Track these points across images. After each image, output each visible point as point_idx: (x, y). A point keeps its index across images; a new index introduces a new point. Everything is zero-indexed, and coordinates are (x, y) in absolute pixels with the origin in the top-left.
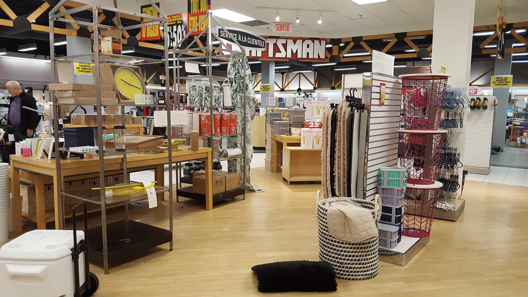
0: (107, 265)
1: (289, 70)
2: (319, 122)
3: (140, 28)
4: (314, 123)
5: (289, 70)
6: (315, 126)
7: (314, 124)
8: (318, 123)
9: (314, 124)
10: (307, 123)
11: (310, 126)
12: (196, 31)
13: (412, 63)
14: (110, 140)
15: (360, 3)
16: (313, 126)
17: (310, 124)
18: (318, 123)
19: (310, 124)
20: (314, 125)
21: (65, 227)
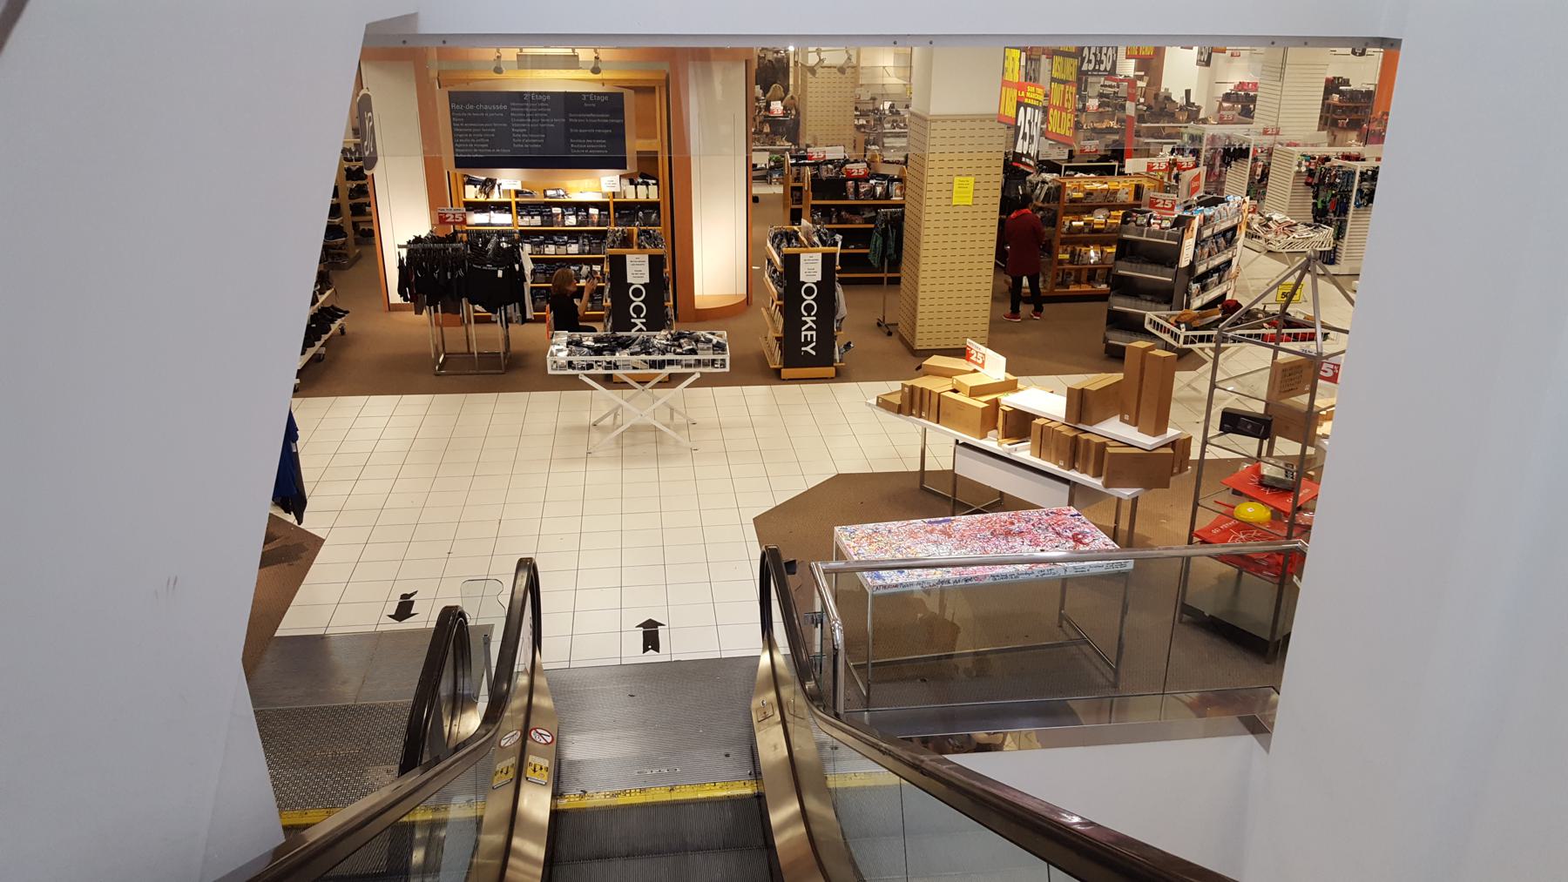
4: (454, 215)
17: (1158, 201)
18: (1332, 367)
19: (1158, 201)
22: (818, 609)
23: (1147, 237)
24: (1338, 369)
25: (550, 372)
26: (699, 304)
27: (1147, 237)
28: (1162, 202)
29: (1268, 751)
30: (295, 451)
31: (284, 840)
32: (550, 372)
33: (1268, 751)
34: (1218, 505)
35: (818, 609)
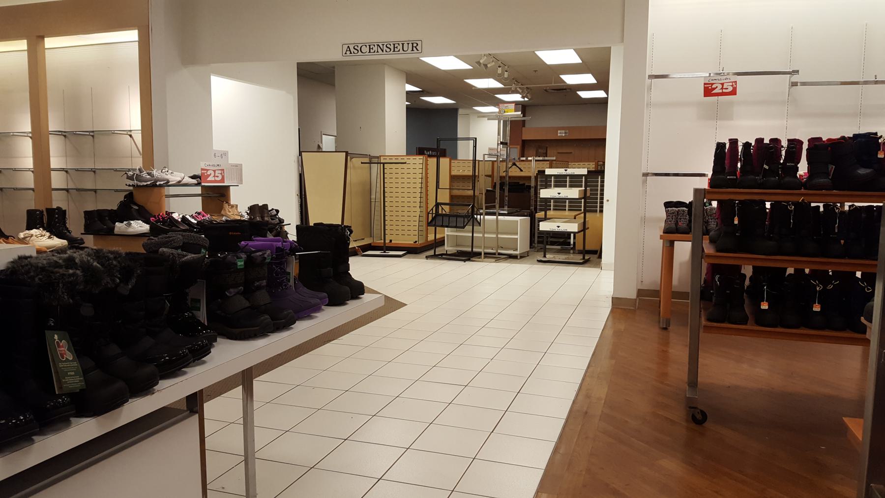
0: (694, 219)
1: (546, 203)
3: (334, 85)
4: (722, 84)
5: (546, 203)
6: (724, 91)
7: (723, 87)
8: (731, 84)
10: (708, 86)
11: (714, 92)
12: (352, 245)
13: (386, 208)
14: (139, 148)
15: (443, 69)
17: (714, 86)
18: (731, 84)
19: (714, 86)
20: (722, 89)
21: (599, 250)
22: (66, 378)
23: (554, 83)
24: (736, 84)
25: (205, 281)
26: (115, 233)
27: (554, 83)
28: (720, 86)
29: (406, 305)
30: (683, 249)
31: (857, 276)
32: (205, 281)
33: (406, 305)
34: (403, 161)
35: (66, 378)
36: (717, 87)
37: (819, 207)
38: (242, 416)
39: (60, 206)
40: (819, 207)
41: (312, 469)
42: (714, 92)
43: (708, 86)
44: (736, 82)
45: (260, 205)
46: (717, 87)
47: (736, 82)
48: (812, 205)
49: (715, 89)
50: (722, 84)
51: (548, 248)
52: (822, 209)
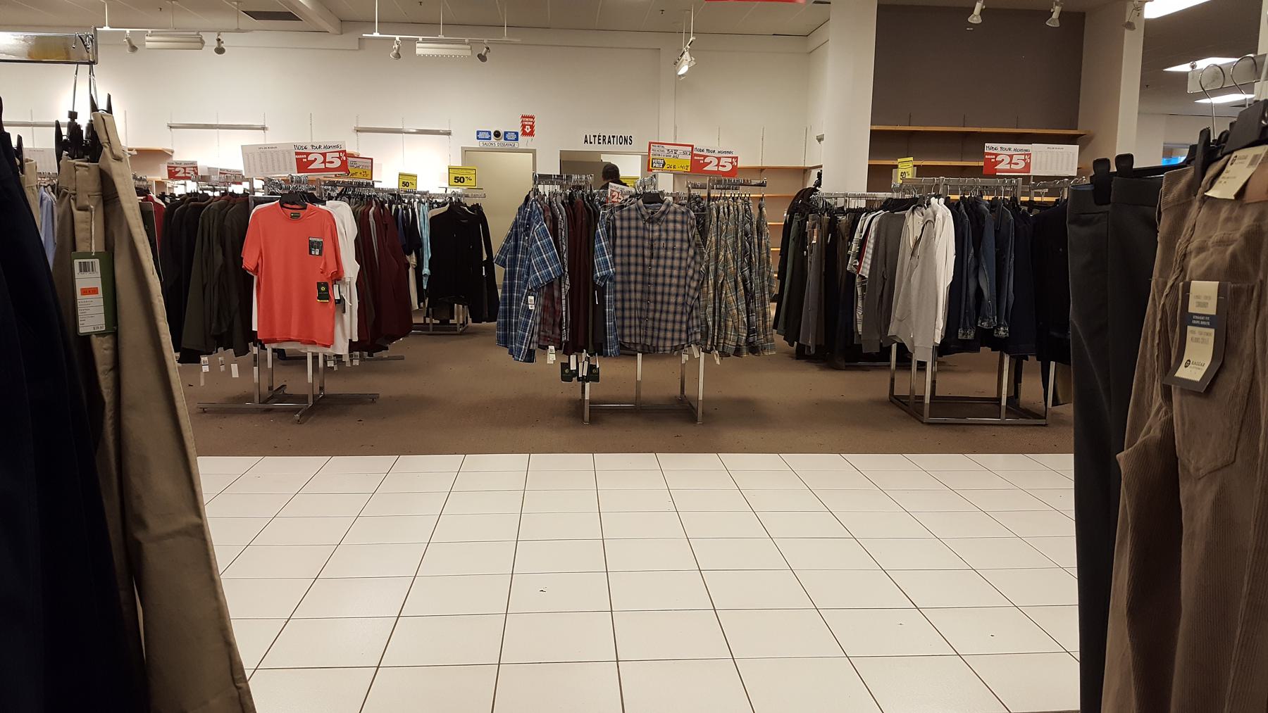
2: (732, 158)
6: (328, 165)
7: (719, 163)
8: (730, 160)
9: (719, 163)
10: (698, 158)
11: (177, 175)
16: (322, 166)
17: (707, 160)
24: (1030, 158)
28: (1007, 160)
36: (316, 159)
37: (473, 322)
38: (249, 683)
39: (601, 175)
40: (473, 322)
41: (255, 668)
42: (177, 175)
43: (698, 158)
44: (737, 158)
45: (990, 349)
46: (316, 159)
47: (737, 158)
48: (1051, 362)
49: (178, 172)
50: (185, 168)
51: (583, 387)
52: (451, 321)
